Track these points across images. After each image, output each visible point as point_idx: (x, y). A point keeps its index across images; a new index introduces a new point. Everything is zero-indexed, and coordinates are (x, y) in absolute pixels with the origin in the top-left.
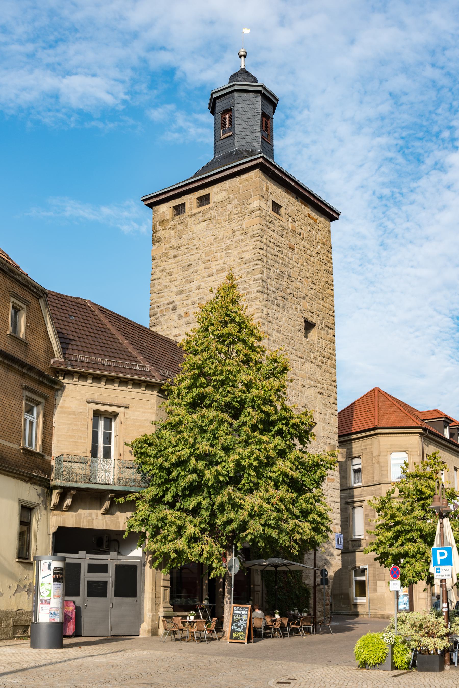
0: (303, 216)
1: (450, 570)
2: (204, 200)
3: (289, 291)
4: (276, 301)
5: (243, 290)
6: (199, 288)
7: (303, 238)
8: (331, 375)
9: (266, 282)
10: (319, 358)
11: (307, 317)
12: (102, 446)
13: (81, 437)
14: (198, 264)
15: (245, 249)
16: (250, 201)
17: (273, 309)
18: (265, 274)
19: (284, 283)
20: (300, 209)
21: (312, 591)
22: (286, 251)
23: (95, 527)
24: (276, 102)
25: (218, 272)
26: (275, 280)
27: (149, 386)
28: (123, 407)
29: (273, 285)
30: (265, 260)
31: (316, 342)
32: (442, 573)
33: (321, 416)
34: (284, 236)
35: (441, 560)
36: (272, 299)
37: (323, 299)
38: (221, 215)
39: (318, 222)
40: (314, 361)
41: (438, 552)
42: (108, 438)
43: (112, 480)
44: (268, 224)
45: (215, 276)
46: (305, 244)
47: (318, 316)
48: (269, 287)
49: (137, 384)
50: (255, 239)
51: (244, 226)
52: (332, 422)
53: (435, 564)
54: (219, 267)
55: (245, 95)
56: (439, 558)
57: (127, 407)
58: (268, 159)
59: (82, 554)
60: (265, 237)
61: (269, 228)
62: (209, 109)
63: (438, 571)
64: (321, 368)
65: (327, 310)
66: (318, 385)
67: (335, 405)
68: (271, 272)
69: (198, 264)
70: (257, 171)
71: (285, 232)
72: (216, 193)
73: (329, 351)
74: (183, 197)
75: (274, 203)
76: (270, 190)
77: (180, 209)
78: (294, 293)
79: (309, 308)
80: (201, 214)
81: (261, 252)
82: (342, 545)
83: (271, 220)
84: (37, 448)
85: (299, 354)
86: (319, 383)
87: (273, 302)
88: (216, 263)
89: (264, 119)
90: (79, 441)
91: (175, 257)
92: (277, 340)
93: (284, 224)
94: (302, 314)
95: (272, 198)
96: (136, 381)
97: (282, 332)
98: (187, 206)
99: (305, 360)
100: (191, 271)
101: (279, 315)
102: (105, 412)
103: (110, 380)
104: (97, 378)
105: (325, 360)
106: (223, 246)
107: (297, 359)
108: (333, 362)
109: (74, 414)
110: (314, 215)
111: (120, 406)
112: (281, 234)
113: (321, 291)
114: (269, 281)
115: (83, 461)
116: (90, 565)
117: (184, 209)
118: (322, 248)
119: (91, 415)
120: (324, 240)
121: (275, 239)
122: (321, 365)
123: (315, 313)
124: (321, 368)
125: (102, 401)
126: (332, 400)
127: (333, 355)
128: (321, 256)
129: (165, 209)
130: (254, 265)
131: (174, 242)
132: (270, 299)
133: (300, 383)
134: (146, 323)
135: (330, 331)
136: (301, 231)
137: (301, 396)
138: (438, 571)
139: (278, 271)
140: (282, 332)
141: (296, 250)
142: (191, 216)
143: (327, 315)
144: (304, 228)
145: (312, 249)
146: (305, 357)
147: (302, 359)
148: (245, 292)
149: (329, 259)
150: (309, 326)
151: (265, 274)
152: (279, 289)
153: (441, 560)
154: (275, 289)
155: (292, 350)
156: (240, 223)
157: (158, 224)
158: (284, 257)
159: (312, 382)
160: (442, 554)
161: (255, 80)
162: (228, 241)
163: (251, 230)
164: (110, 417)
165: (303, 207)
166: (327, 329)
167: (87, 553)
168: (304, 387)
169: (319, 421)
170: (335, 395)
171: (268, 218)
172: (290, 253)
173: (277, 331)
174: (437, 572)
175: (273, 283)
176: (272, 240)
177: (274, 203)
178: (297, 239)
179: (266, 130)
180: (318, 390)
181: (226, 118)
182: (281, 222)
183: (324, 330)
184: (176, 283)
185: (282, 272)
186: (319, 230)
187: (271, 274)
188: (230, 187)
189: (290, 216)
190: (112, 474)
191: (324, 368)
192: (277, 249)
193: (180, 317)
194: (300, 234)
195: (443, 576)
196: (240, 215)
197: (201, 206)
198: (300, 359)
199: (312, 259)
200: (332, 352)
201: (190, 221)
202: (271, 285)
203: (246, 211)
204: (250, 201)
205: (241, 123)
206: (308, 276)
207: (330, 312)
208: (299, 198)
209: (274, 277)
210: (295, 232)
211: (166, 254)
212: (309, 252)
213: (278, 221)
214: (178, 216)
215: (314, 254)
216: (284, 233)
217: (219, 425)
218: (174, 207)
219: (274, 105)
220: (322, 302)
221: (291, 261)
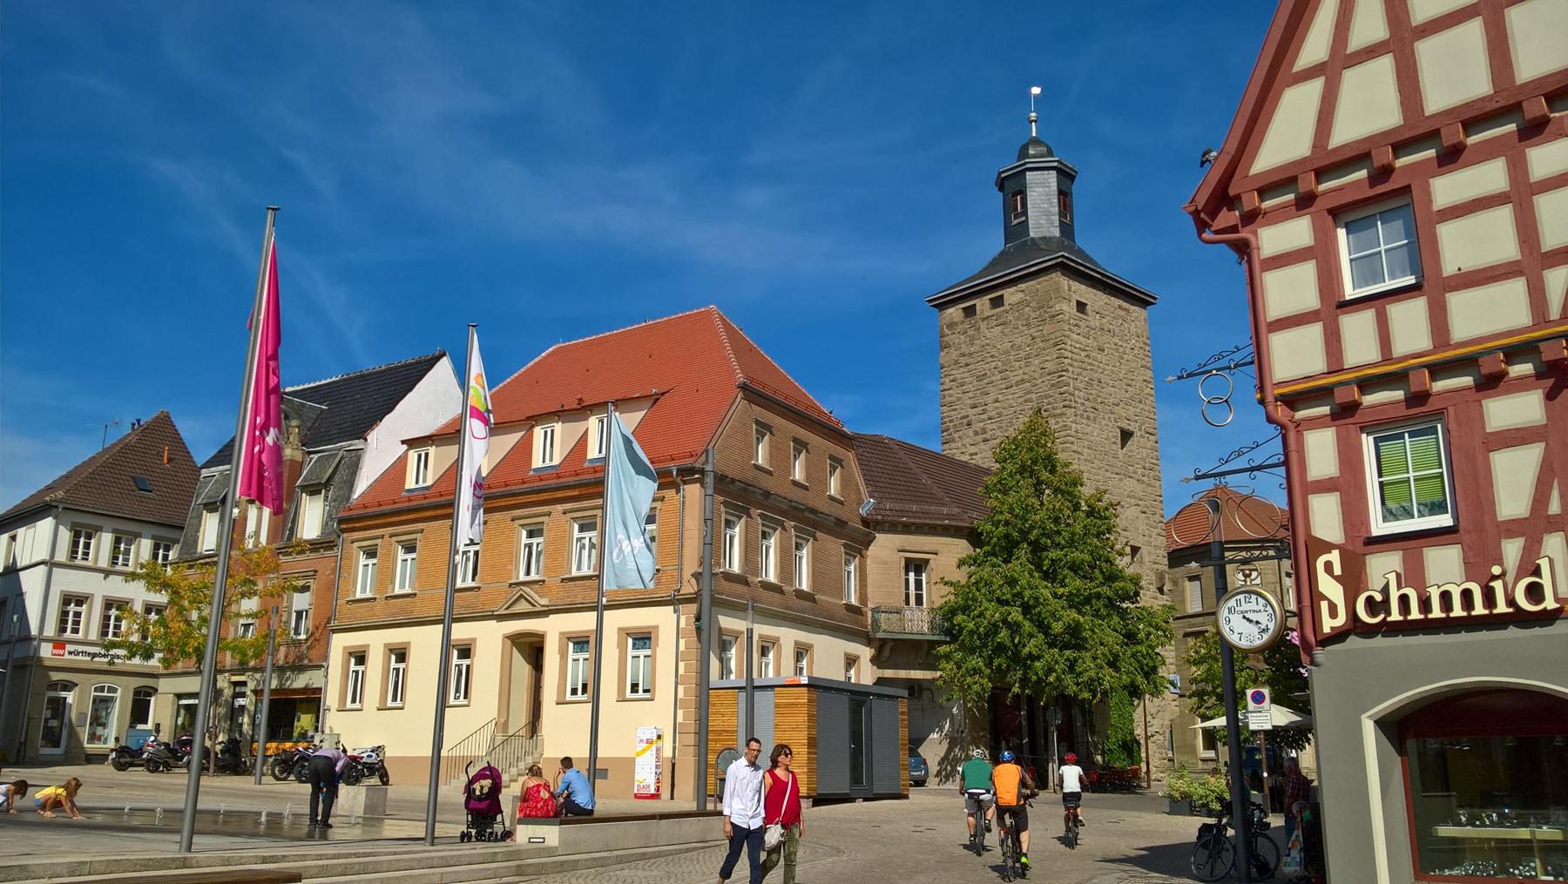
21: (1142, 742)
25: (1017, 384)
38: (1018, 319)
72: (1011, 295)
77: (970, 312)
84: (854, 601)
95: (1076, 297)
106: (1022, 354)
110: (1126, 305)
129: (954, 312)
131: (964, 349)
134: (935, 446)
150: (1126, 435)
178: (1107, 337)
187: (1078, 384)
193: (976, 433)
201: (983, 325)
217: (1015, 833)
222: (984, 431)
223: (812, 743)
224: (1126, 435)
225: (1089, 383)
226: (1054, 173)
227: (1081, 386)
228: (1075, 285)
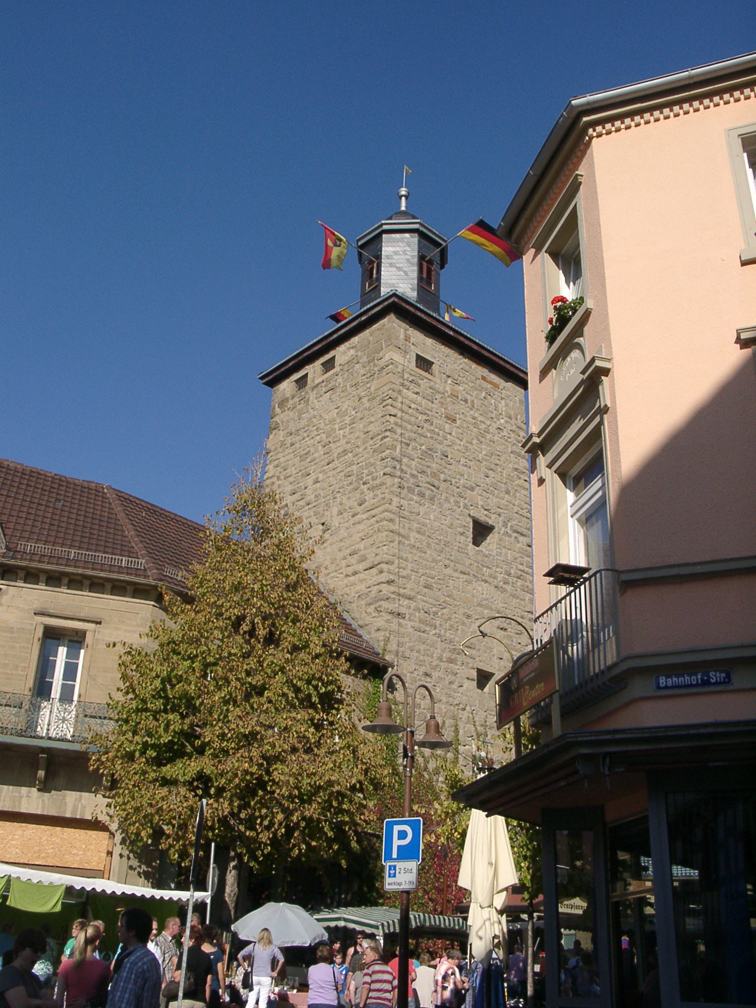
0: (473, 378)
2: (329, 365)
3: (442, 477)
5: (367, 475)
6: (316, 482)
8: (523, 602)
9: (400, 462)
10: (500, 577)
11: (477, 515)
12: (60, 683)
14: (317, 451)
15: (372, 419)
16: (381, 355)
18: (398, 450)
19: (434, 465)
20: (467, 368)
27: (139, 591)
28: (93, 622)
29: (413, 466)
30: (399, 431)
31: (495, 553)
35: (398, 846)
37: (508, 492)
39: (501, 387)
40: (491, 580)
41: (396, 828)
42: (70, 672)
43: (45, 731)
44: (408, 384)
45: (336, 462)
46: (476, 415)
47: (499, 515)
48: (404, 467)
49: (119, 588)
50: (384, 404)
51: (372, 389)
54: (340, 450)
55: (398, 236)
56: (396, 842)
57: (100, 623)
60: (400, 399)
64: (504, 591)
65: (516, 509)
68: (410, 447)
69: (317, 451)
70: (392, 317)
71: (438, 396)
72: (342, 354)
73: (520, 567)
75: (419, 358)
76: (412, 340)
77: (302, 382)
79: (480, 503)
80: (324, 384)
81: (392, 419)
85: (460, 567)
87: (410, 490)
88: (338, 444)
90: (14, 672)
91: (292, 444)
92: (417, 545)
93: (437, 386)
94: (468, 512)
97: (427, 533)
100: (308, 460)
101: (422, 510)
102: (64, 629)
103: (75, 582)
104: (54, 579)
108: (528, 584)
109: (12, 632)
110: (493, 377)
111: (88, 621)
112: (430, 398)
113: (505, 480)
114: (405, 460)
118: (506, 422)
119: (40, 633)
120: (512, 413)
121: (420, 405)
122: (504, 586)
123: (492, 511)
124: (504, 591)
128: (505, 433)
129: (287, 386)
130: (382, 439)
131: (292, 427)
132: (406, 485)
133: (461, 611)
136: (469, 397)
137: (463, 630)
139: (423, 447)
140: (427, 533)
141: (458, 422)
142: (313, 389)
146: (472, 573)
147: (465, 576)
148: (370, 477)
150: (481, 531)
151: (398, 450)
152: (423, 472)
153: (398, 846)
155: (447, 561)
156: (368, 385)
158: (436, 430)
159: (486, 611)
160: (402, 835)
162: (353, 413)
163: (380, 393)
164: (76, 640)
165: (474, 366)
166: (515, 535)
168: (469, 617)
169: (499, 670)
171: (406, 376)
173: (419, 532)
176: (413, 406)
177: (419, 358)
178: (461, 407)
183: (510, 536)
184: (291, 479)
185: (431, 450)
186: (502, 399)
189: (449, 377)
190: (46, 722)
191: (510, 591)
194: (466, 401)
195: (400, 884)
196: (369, 375)
198: (461, 576)
199: (489, 436)
201: (312, 396)
202: (409, 466)
203: (376, 369)
204: (381, 355)
205: (390, 269)
206: (480, 458)
209: (416, 455)
211: (283, 444)
212: (483, 426)
215: (492, 430)
220: (507, 496)
221: (449, 436)
223: (238, 992)
224: (481, 531)
225: (429, 453)
226: (414, 239)
228: (417, 336)
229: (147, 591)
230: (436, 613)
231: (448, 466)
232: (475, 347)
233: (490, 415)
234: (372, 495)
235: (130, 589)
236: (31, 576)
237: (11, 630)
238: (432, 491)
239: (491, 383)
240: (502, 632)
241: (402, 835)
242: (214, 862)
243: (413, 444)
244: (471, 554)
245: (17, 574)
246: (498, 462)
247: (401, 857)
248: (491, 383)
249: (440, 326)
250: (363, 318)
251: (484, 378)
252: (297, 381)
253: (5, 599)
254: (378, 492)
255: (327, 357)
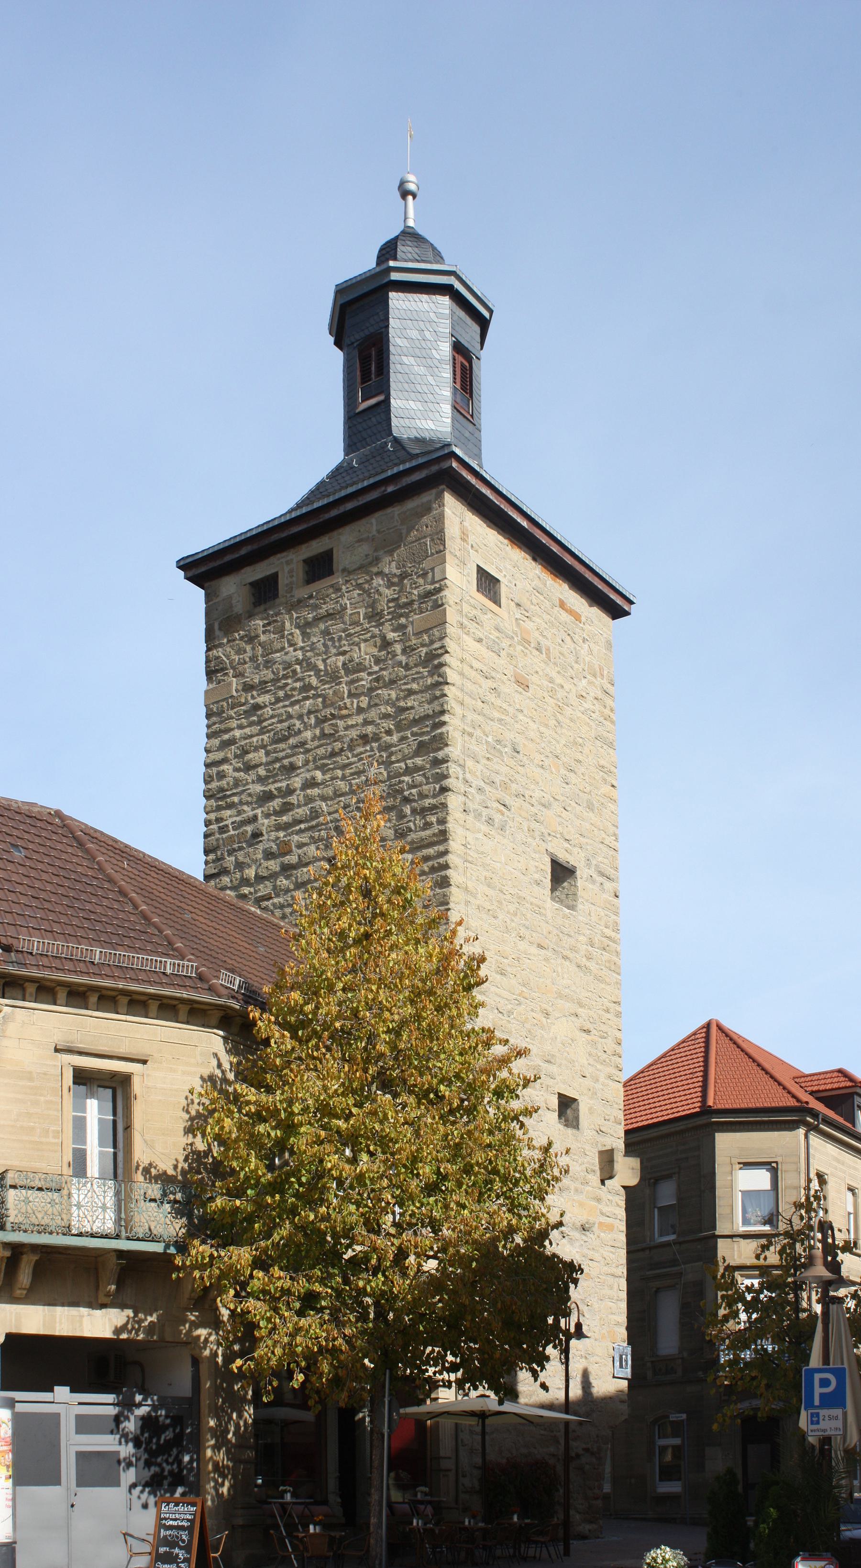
1: (840, 1417)
4: (485, 812)
7: (549, 657)
13: (47, 1131)
17: (479, 831)
22: (507, 691)
23: (57, 1333)
24: (486, 314)
26: (485, 761)
29: (478, 774)
32: (823, 1425)
33: (587, 1082)
34: (503, 653)
35: (821, 1395)
36: (476, 807)
39: (583, 619)
41: (817, 1377)
46: (554, 674)
48: (468, 776)
52: (610, 1098)
53: (810, 1405)
56: (818, 1391)
57: (144, 1062)
58: (467, 459)
59: (62, 1392)
61: (468, 634)
62: (330, 334)
63: (815, 1419)
66: (580, 1011)
67: (616, 1058)
73: (606, 931)
74: (273, 559)
75: (480, 571)
76: (471, 539)
78: (527, 793)
82: (629, 1370)
83: (474, 612)
86: (581, 1005)
87: (478, 816)
89: (460, 359)
90: (44, 1140)
94: (544, 845)
96: (165, 1001)
98: (283, 581)
99: (549, 953)
102: (100, 1072)
103: (108, 1000)
104: (78, 996)
105: (596, 952)
107: (534, 950)
109: (31, 1079)
112: (496, 648)
115: (54, 1185)
116: (79, 1418)
117: (277, 589)
125: (81, 1046)
126: (610, 1045)
127: (615, 942)
129: (233, 587)
135: (608, 885)
138: (815, 1419)
143: (601, 846)
144: (549, 636)
145: (567, 687)
147: (544, 951)
149: (607, 712)
150: (561, 873)
153: (821, 1395)
154: (482, 784)
157: (216, 626)
160: (825, 1383)
161: (438, 257)
166: (600, 879)
167: (72, 1391)
170: (618, 1034)
171: (466, 608)
172: (517, 696)
174: (812, 1423)
175: (479, 767)
178: (535, 661)
179: (463, 388)
180: (578, 1022)
181: (370, 356)
182: (499, 620)
183: (594, 882)
188: (378, 532)
192: (487, 684)
195: (825, 1431)
197: (313, 581)
199: (568, 711)
200: (613, 934)
203: (415, 592)
207: (609, 840)
208: (538, 559)
210: (529, 643)
213: (490, 615)
214: (262, 607)
216: (503, 645)
218: (251, 584)
219: (484, 324)
222: (285, 849)
227: (480, 750)
229: (204, 1011)
230: (510, 1013)
231: (520, 769)
232: (555, 548)
233: (571, 672)
234: (420, 822)
235: (183, 1010)
236: (45, 991)
237: (29, 1076)
238: (503, 814)
239: (571, 612)
240: (584, 1035)
241: (825, 1383)
242: (390, 1395)
243: (478, 733)
244: (549, 914)
245: (24, 990)
246: (581, 758)
247: (823, 1405)
248: (571, 612)
249: (465, 474)
250: (390, 489)
251: (562, 605)
252: (254, 585)
253: (12, 1028)
254: (433, 819)
255: (316, 547)
